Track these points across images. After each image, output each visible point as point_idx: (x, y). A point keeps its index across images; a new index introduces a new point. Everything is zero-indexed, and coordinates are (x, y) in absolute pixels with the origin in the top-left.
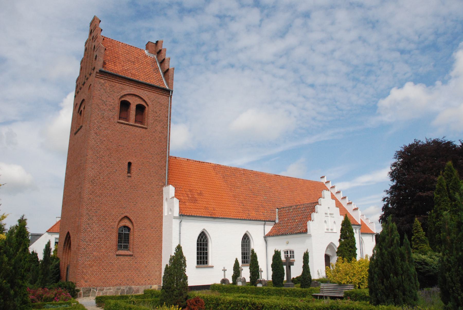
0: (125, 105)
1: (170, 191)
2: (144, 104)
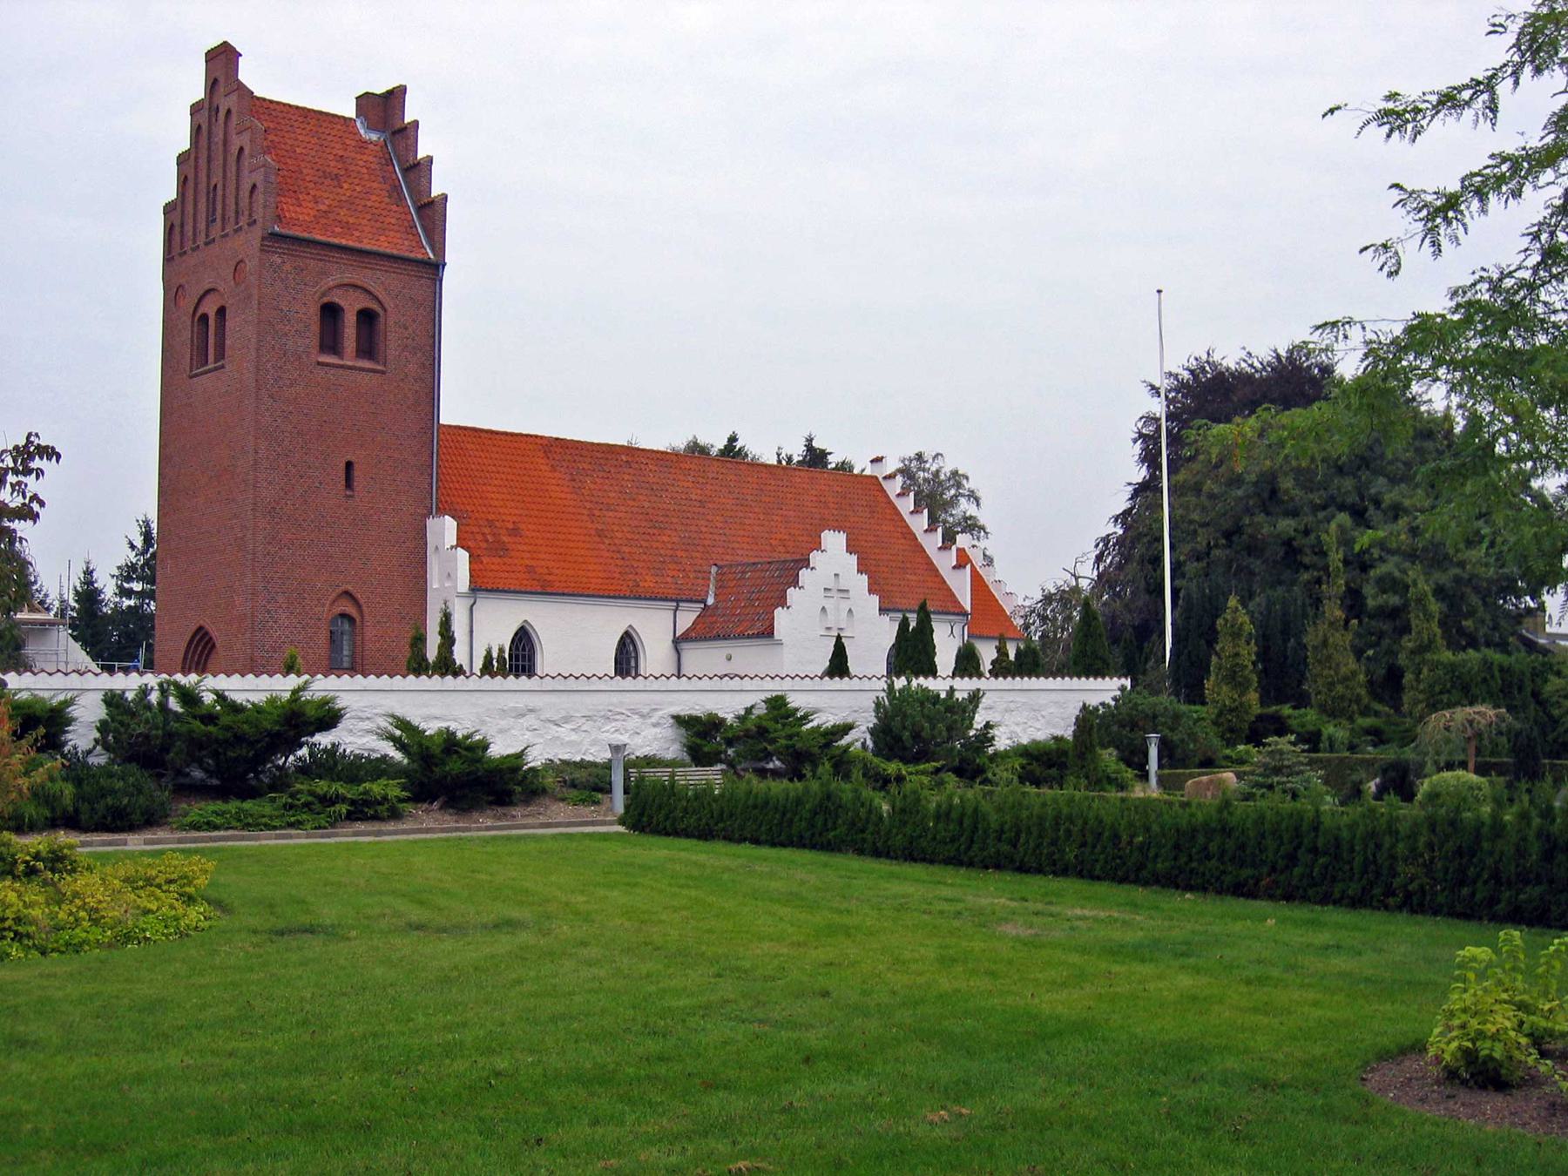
0: (331, 312)
1: (444, 530)
2: (374, 306)
